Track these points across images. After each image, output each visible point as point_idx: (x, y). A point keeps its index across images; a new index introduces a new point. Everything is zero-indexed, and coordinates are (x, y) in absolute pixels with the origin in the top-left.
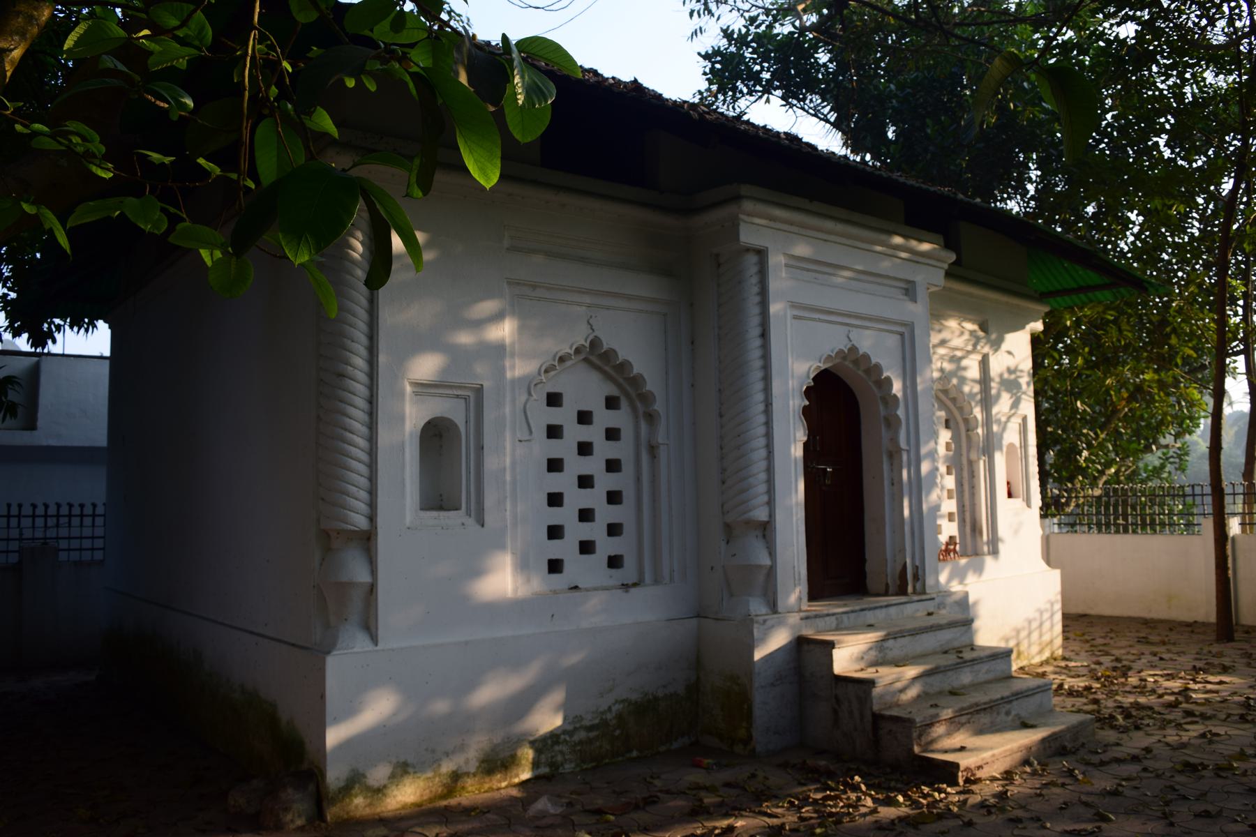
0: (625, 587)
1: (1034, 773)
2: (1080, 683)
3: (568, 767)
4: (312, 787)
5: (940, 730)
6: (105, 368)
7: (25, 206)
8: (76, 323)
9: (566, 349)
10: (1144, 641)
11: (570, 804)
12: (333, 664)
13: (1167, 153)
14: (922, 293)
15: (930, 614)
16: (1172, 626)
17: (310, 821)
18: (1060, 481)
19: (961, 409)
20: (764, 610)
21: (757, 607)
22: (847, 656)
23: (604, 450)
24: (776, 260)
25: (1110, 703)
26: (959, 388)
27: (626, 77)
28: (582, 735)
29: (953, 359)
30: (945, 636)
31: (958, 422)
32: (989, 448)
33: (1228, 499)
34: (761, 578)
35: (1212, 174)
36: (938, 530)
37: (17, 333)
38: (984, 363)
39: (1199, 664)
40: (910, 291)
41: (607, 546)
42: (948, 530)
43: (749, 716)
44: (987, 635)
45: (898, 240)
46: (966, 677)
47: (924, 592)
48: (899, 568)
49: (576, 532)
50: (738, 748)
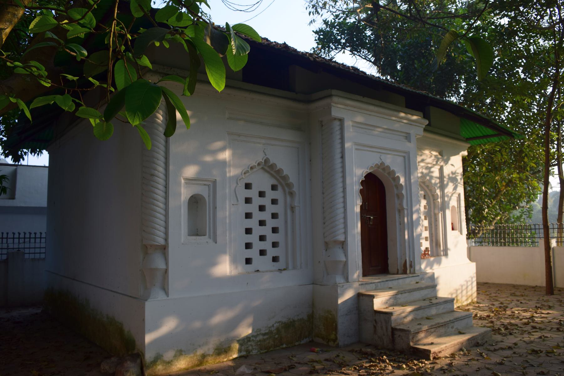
0: (280, 270)
1: (464, 355)
2: (485, 314)
3: (254, 352)
4: (139, 361)
5: (422, 335)
7: (11, 99)
8: (33, 151)
10: (513, 294)
11: (255, 369)
12: (148, 305)
13: (522, 76)
14: (413, 138)
15: (417, 283)
18: (475, 222)
19: (431, 190)
21: (339, 279)
24: (348, 124)
25: (498, 323)
27: (281, 42)
28: (261, 337)
29: (427, 168)
30: (424, 293)
31: (430, 196)
35: (543, 85)
36: (420, 245)
37: (7, 156)
38: (441, 170)
39: (538, 305)
40: (408, 137)
41: (271, 252)
42: (425, 244)
43: (336, 329)
44: (443, 292)
45: (402, 115)
46: (433, 311)
47: (414, 273)
48: (403, 262)
49: (258, 246)
50: (331, 343)
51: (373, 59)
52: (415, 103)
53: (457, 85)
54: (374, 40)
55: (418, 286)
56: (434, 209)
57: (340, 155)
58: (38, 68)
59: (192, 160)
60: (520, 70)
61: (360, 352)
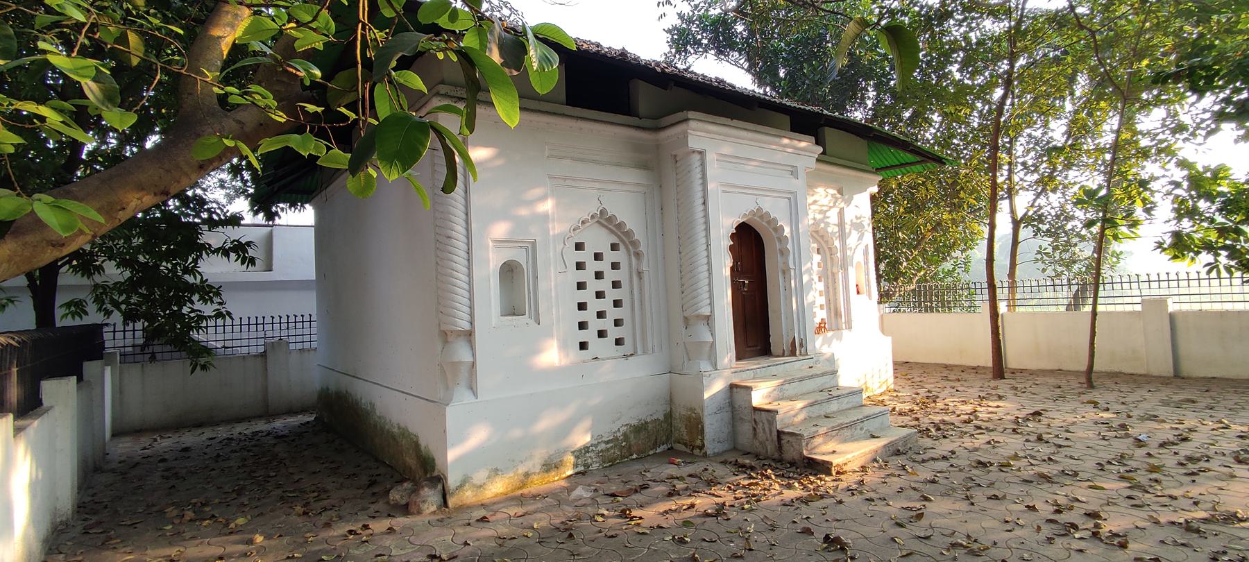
0: (626, 356)
1: (881, 467)
2: (906, 407)
3: (595, 466)
4: (440, 487)
5: (818, 440)
6: (311, 233)
7: (225, 141)
8: (293, 205)
9: (586, 216)
10: (946, 378)
11: (596, 490)
12: (450, 411)
13: (958, 76)
14: (801, 173)
16: (964, 369)
17: (439, 508)
18: (888, 280)
19: (827, 242)
20: (709, 368)
21: (705, 366)
22: (759, 397)
23: (611, 276)
24: (711, 157)
25: (926, 420)
26: (825, 229)
27: (617, 46)
28: (603, 446)
29: (821, 212)
30: (820, 381)
31: (825, 249)
32: (844, 267)
33: (998, 291)
34: (707, 348)
35: (990, 85)
36: (814, 315)
37: (256, 213)
38: (841, 213)
39: (982, 394)
40: (794, 172)
41: (614, 332)
42: (821, 315)
44: (846, 380)
45: (786, 141)
46: (834, 406)
49: (595, 324)
50: (697, 452)
51: (746, 65)
52: (804, 124)
53: (863, 95)
54: (748, 39)
55: (812, 372)
56: (832, 265)
57: (701, 201)
58: (262, 96)
59: (502, 214)
60: (954, 68)
61: (736, 464)
